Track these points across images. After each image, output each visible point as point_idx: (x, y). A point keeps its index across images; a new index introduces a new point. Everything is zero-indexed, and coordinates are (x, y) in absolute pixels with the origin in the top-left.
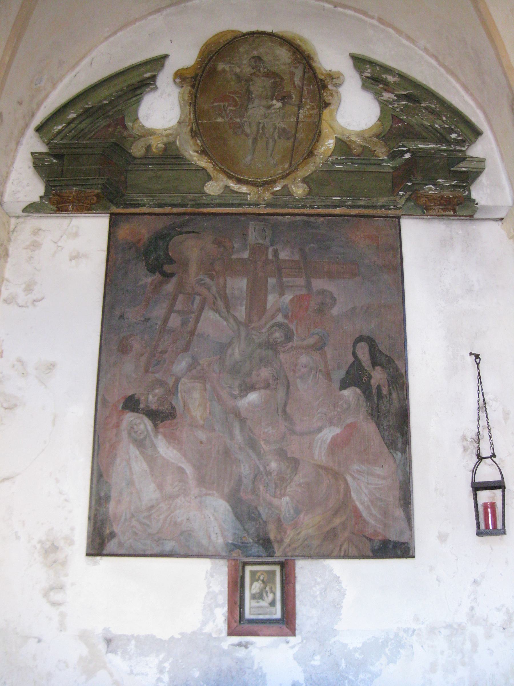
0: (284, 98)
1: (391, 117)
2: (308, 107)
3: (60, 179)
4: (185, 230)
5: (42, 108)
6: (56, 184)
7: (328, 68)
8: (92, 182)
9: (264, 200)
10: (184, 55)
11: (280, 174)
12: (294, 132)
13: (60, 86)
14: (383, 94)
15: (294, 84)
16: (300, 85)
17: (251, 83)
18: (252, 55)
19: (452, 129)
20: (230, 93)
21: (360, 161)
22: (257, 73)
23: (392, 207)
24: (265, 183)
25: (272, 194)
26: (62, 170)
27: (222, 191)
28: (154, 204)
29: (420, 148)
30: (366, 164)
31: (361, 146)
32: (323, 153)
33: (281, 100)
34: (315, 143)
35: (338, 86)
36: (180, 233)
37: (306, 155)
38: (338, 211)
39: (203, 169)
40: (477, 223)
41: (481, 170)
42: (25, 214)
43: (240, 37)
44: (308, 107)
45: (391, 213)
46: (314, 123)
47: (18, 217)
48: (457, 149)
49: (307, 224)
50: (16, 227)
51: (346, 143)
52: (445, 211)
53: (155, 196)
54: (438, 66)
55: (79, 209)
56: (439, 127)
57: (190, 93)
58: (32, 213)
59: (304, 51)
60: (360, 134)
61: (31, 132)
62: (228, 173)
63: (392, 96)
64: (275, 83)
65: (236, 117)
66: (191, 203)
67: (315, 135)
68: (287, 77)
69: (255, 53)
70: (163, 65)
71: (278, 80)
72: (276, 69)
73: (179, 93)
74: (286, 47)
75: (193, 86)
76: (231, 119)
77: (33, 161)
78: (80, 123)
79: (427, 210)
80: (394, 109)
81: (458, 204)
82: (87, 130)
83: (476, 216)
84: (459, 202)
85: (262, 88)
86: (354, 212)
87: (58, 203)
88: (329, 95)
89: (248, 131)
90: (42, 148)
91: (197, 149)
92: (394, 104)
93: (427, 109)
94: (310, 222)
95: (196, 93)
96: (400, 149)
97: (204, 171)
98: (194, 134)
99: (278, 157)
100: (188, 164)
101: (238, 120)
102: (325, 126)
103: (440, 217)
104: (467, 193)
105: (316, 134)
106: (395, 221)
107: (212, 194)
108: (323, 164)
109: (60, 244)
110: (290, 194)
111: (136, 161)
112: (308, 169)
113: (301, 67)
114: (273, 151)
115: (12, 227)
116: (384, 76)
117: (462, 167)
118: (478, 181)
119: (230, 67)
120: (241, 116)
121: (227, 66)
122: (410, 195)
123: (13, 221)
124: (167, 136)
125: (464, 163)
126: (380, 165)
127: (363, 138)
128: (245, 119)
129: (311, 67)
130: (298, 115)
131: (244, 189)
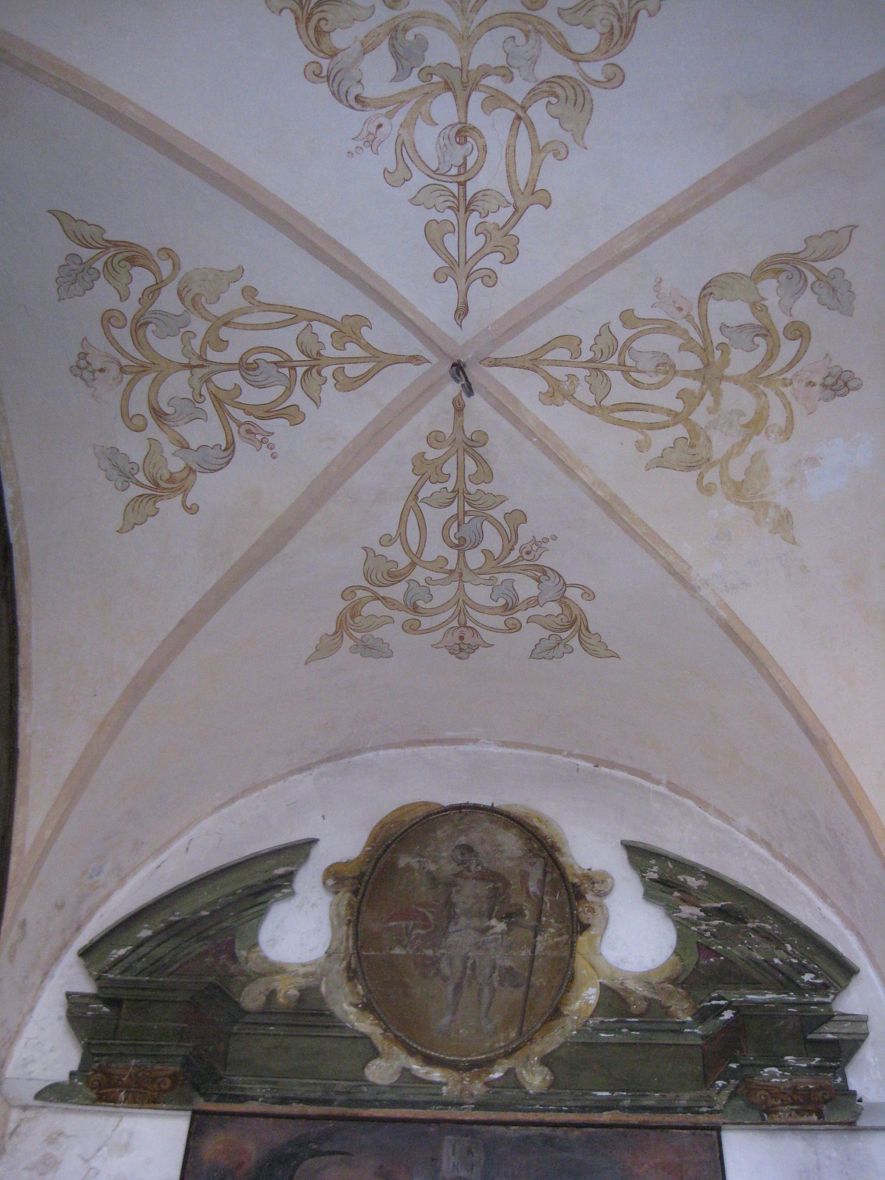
0: (511, 916)
1: (695, 945)
2: (552, 930)
3: (109, 1042)
4: (326, 1147)
5: (96, 917)
6: (103, 1050)
7: (586, 866)
8: (165, 1051)
9: (472, 1095)
10: (344, 841)
11: (501, 1048)
12: (527, 974)
13: (132, 883)
14: (681, 907)
15: (528, 892)
16: (539, 893)
17: (454, 889)
18: (457, 843)
19: (804, 966)
20: (419, 905)
21: (645, 1026)
22: (466, 873)
23: (705, 1109)
24: (473, 1065)
25: (487, 1084)
26: (117, 1027)
27: (396, 1078)
29: (751, 1001)
30: (654, 1031)
31: (645, 998)
32: (579, 1011)
33: (505, 918)
34: (564, 994)
35: (602, 895)
36: (316, 1154)
38: (606, 1117)
39: (365, 1037)
40: (863, 1136)
41: (861, 1037)
42: (38, 1103)
43: (438, 813)
45: (703, 1119)
47: (25, 1108)
48: (816, 1000)
49: (548, 1141)
50: (17, 1127)
51: (619, 996)
52: (802, 1115)
53: (275, 1083)
54: (772, 860)
55: (137, 1099)
56: (780, 963)
57: (349, 904)
58: (51, 1101)
59: (546, 838)
60: (644, 978)
61: (71, 956)
62: (408, 1044)
63: (696, 911)
64: (495, 889)
65: (428, 948)
67: (564, 979)
69: (463, 840)
70: (307, 856)
71: (500, 884)
73: (331, 904)
74: (514, 831)
75: (355, 893)
76: (418, 950)
77: (67, 1007)
78: (159, 945)
79: (768, 1114)
80: (700, 934)
81: (826, 1102)
83: (862, 1122)
84: (826, 1097)
89: (447, 971)
90: (85, 985)
92: (700, 924)
93: (757, 932)
96: (714, 1002)
98: (352, 974)
100: (340, 1027)
101: (430, 952)
102: (581, 966)
103: (794, 1127)
104: (839, 1080)
105: (566, 978)
106: (711, 1135)
108: (578, 1031)
109: (94, 1163)
111: (248, 1019)
112: (552, 1040)
113: (539, 864)
115: (11, 1126)
116: (681, 878)
117: (828, 1033)
118: (858, 1057)
121: (414, 860)
122: (737, 1087)
123: (15, 1115)
124: (306, 975)
125: (830, 1024)
126: (679, 1032)
128: (442, 951)
131: (436, 1075)
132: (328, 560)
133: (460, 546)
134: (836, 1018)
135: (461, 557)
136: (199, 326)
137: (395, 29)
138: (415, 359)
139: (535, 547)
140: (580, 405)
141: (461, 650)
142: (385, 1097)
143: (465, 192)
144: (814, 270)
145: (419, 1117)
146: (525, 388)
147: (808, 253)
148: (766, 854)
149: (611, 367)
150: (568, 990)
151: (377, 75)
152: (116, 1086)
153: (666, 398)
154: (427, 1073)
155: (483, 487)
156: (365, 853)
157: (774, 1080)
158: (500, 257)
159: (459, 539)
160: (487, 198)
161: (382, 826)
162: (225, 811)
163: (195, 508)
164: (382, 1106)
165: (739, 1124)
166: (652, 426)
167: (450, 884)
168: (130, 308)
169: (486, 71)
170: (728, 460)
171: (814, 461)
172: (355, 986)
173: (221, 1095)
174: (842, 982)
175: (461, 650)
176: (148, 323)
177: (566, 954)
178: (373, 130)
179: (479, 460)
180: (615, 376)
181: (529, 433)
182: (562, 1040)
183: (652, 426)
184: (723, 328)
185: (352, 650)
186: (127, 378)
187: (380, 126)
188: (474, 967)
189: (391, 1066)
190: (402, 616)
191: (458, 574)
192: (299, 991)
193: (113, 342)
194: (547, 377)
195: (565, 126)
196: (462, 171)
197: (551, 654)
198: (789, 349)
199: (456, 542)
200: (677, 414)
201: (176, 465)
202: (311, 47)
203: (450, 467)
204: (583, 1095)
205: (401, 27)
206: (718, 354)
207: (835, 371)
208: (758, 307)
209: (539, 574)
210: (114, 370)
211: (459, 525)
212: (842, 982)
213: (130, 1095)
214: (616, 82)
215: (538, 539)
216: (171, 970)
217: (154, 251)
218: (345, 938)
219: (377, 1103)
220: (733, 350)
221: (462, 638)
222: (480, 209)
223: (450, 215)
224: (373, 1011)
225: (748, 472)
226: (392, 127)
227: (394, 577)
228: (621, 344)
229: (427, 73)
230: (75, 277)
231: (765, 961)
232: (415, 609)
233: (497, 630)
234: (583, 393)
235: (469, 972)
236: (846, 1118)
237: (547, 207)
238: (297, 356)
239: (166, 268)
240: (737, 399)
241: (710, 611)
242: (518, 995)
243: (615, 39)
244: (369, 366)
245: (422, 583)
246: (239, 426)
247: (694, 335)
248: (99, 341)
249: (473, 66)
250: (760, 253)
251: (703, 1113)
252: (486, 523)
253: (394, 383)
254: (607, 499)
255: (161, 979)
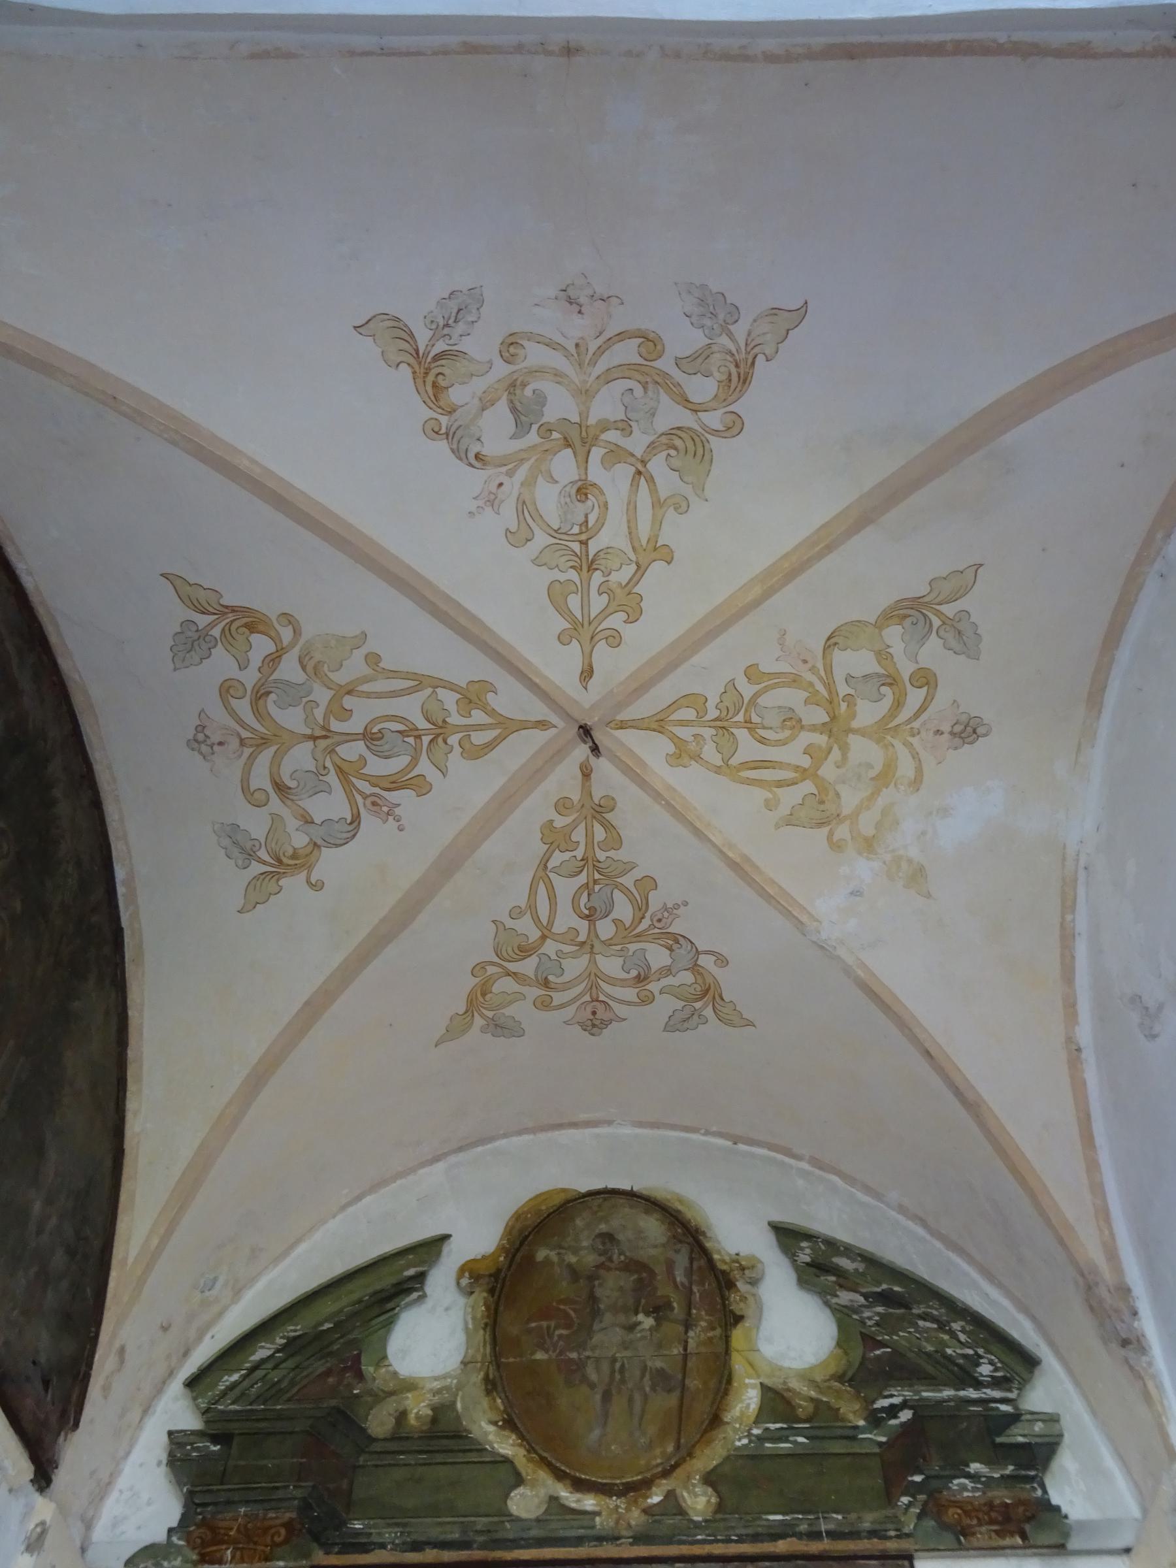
0: (659, 1310)
2: (703, 1324)
3: (215, 1488)
7: (733, 1252)
8: (280, 1494)
9: (629, 1525)
10: (477, 1236)
11: (658, 1465)
12: (680, 1376)
13: (249, 1296)
15: (675, 1282)
17: (596, 1283)
18: (597, 1231)
20: (561, 1301)
22: (608, 1264)
25: (646, 1511)
28: (404, 1543)
30: (823, 1438)
31: (812, 1399)
33: (653, 1312)
35: (754, 1282)
37: (707, 1422)
38: (782, 1546)
39: (507, 1461)
43: (576, 1199)
45: (892, 1546)
51: (783, 1397)
53: (405, 1525)
54: (928, 1237)
60: (806, 1376)
61: (176, 1386)
64: (640, 1280)
65: (572, 1350)
66: (481, 1539)
67: (720, 1382)
68: (660, 1269)
69: (603, 1227)
70: (438, 1254)
71: (644, 1275)
74: (655, 1215)
75: (491, 1291)
76: (561, 1353)
79: (965, 1536)
81: (1029, 1519)
82: (284, 1385)
83: (1073, 1544)
86: (815, 1547)
87: (204, 1544)
89: (593, 1377)
90: (190, 1421)
91: (495, 1418)
98: (491, 1386)
99: (652, 1430)
102: (738, 1364)
105: (722, 1382)
106: (903, 1566)
107: (524, 1515)
110: (681, 1512)
112: (710, 1457)
113: (685, 1250)
114: (641, 1418)
117: (1017, 1435)
118: (1055, 1465)
119: (559, 1254)
120: (582, 1346)
122: (925, 1504)
124: (438, 1392)
125: (1019, 1425)
126: (853, 1438)
127: (813, 1383)
128: (588, 1353)
131: (589, 1502)
132: (457, 937)
133: (590, 917)
134: (1023, 1418)
135: (592, 929)
136: (322, 696)
137: (513, 385)
138: (542, 725)
139: (666, 914)
140: (707, 765)
141: (594, 1026)
143: (587, 552)
144: (939, 614)
146: (653, 751)
147: (932, 596)
148: (921, 1231)
149: (737, 725)
150: (726, 1393)
151: (496, 432)
152: (222, 1542)
153: (793, 754)
154: (578, 1501)
155: (611, 853)
156: (501, 1248)
157: (966, 1494)
158: (623, 616)
159: (589, 909)
160: (608, 556)
161: (518, 1216)
162: (351, 1210)
163: (319, 883)
164: (528, 1546)
165: (933, 1550)
166: (780, 784)
167: (591, 1278)
168: (250, 677)
169: (605, 426)
170: (858, 815)
171: (945, 812)
172: (495, 1401)
173: (343, 1544)
174: (1025, 1375)
175: (594, 1026)
176: (268, 693)
177: (720, 1349)
178: (494, 489)
179: (608, 826)
180: (742, 734)
181: (657, 796)
182: (724, 1453)
183: (780, 784)
184: (849, 679)
185: (483, 1030)
186: (247, 751)
187: (501, 485)
188: (622, 1369)
190: (536, 992)
191: (587, 946)
192: (432, 1410)
193: (233, 714)
194: (674, 738)
195: (685, 479)
196: (584, 529)
197: (686, 1025)
198: (916, 696)
199: (587, 912)
200: (805, 770)
201: (300, 840)
202: (428, 400)
203: (579, 835)
205: (518, 383)
206: (844, 706)
207: (964, 718)
208: (883, 655)
209: (671, 942)
210: (234, 743)
211: (589, 895)
212: (1025, 1375)
213: (238, 1553)
214: (735, 430)
215: (670, 905)
216: (288, 1395)
217: (274, 619)
220: (859, 701)
221: (594, 1013)
222: (602, 568)
223: (573, 575)
225: (878, 826)
226: (513, 486)
227: (525, 951)
228: (746, 702)
229: (546, 430)
230: (191, 645)
231: (936, 1351)
232: (546, 984)
233: (629, 1003)
234: (710, 752)
235: (618, 1376)
236: (1054, 1539)
237: (669, 563)
238: (422, 724)
239: (286, 634)
240: (864, 751)
241: (847, 970)
242: (673, 1400)
243: (733, 387)
244: (494, 733)
245: (554, 957)
246: (365, 799)
247: (820, 687)
248: (218, 715)
249: (592, 421)
250: (885, 599)
251: (891, 1538)
252: (616, 893)
253: (521, 749)
254: (738, 860)
255: (279, 1407)
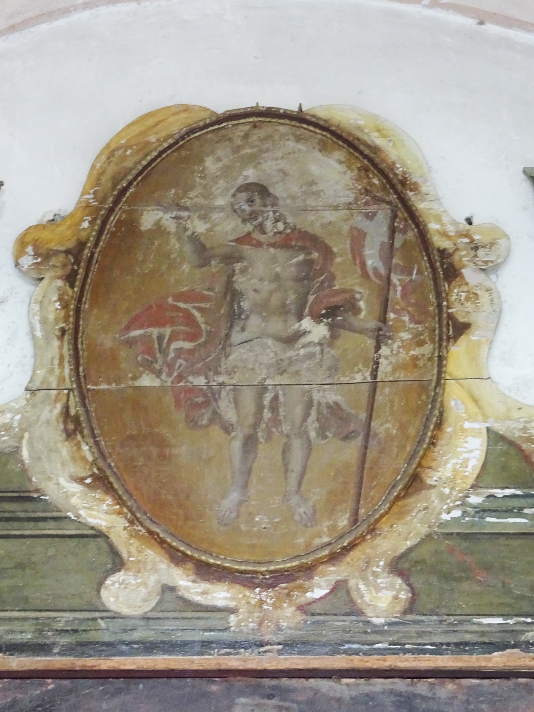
0: (336, 312)
9: (279, 629)
12: (363, 416)
15: (363, 265)
16: (383, 271)
17: (238, 266)
18: (240, 181)
20: (179, 297)
22: (257, 236)
33: (325, 316)
35: (488, 269)
38: (497, 660)
39: (98, 535)
43: (206, 126)
44: (406, 336)
46: (423, 388)
51: (520, 450)
59: (392, 167)
64: (308, 263)
65: (197, 373)
68: (340, 247)
69: (250, 174)
71: (316, 255)
72: (312, 223)
75: (70, 278)
76: (180, 377)
85: (271, 281)
88: (467, 299)
89: (230, 414)
94: (415, 695)
95: (79, 300)
97: (100, 541)
98: (73, 426)
99: (317, 495)
101: (200, 381)
102: (455, 398)
105: (430, 422)
107: (125, 611)
112: (402, 534)
113: (383, 214)
114: (303, 474)
119: (177, 218)
121: (168, 216)
128: (221, 379)
129: (414, 217)
130: (377, 363)
131: (220, 595)
142: (136, 635)
145: (187, 667)
154: (204, 593)
161: (110, 153)
172: (78, 446)
182: (424, 530)
189: (144, 584)
204: (461, 623)
218: (56, 362)
219: (124, 648)
224: (109, 489)
242: (350, 452)
